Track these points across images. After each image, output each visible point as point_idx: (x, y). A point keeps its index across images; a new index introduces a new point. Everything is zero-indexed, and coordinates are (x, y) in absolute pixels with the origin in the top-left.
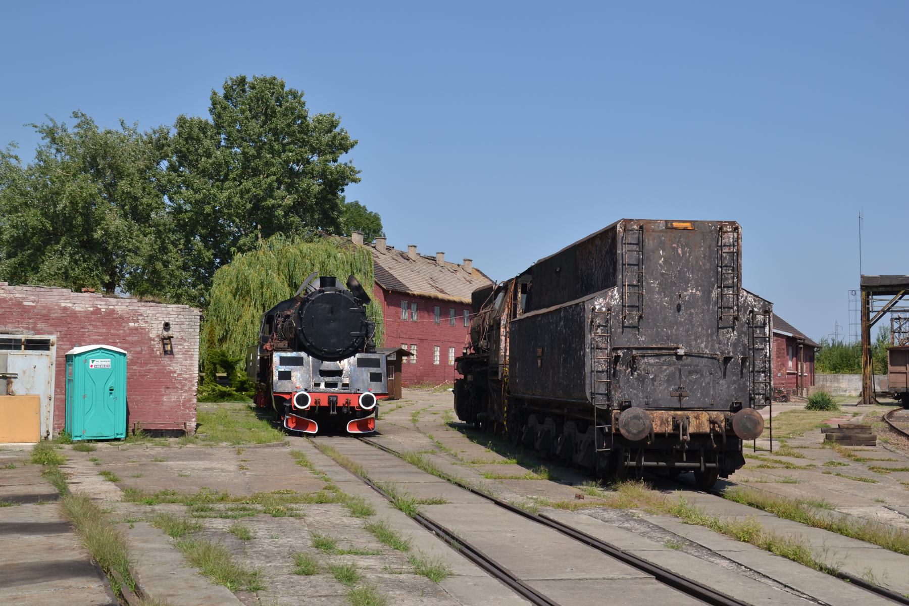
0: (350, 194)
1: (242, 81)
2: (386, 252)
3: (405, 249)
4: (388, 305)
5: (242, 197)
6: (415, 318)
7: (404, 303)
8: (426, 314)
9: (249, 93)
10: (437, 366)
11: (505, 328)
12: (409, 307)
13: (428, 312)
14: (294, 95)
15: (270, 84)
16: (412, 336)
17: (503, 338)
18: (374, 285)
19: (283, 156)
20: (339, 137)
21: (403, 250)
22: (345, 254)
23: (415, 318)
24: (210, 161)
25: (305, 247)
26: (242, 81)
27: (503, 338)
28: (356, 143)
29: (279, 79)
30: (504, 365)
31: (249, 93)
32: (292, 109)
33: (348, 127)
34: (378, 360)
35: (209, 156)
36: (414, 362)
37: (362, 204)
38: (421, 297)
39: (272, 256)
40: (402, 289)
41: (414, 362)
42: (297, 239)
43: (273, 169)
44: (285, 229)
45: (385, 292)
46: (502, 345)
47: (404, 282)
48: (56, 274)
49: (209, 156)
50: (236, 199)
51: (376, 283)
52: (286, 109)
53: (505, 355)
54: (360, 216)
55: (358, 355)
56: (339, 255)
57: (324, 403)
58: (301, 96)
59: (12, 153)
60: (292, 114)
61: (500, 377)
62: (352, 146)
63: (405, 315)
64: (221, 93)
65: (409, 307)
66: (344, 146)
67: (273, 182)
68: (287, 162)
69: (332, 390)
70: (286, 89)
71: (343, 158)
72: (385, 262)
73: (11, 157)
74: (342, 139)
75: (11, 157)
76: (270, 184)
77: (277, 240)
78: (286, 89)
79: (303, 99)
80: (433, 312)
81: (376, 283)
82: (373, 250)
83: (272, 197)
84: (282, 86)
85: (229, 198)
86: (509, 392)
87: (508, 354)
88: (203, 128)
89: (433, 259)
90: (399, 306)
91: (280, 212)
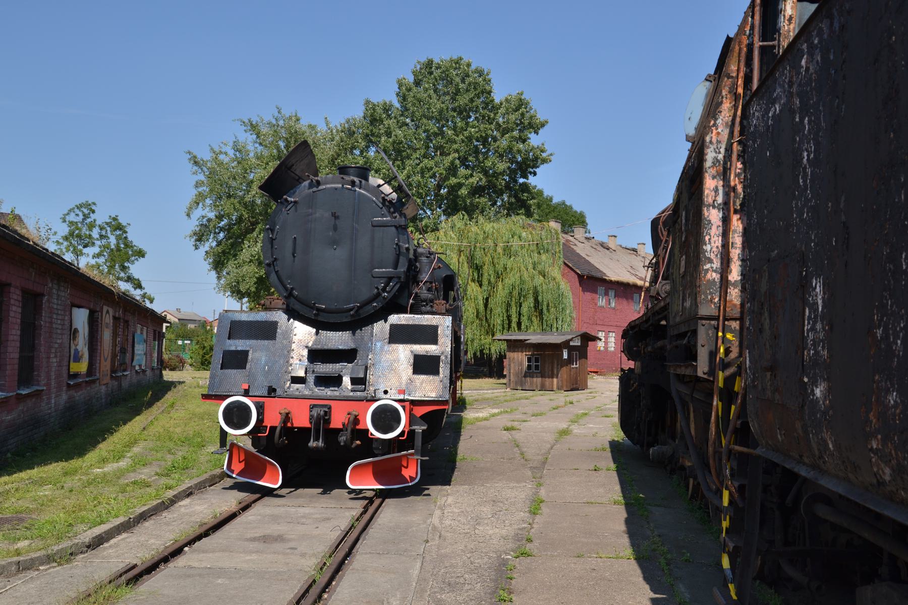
0: (541, 180)
1: (430, 63)
2: (585, 241)
3: (605, 239)
4: (584, 291)
5: (423, 177)
6: (613, 305)
7: (601, 289)
8: (625, 302)
9: (436, 73)
10: (613, 352)
11: (724, 174)
12: (606, 294)
13: (627, 299)
14: (480, 73)
15: (456, 63)
16: (610, 323)
17: (714, 216)
18: (562, 266)
19: (466, 133)
20: (528, 115)
21: (604, 241)
22: (531, 233)
23: (613, 305)
24: (391, 140)
25: (488, 227)
26: (430, 63)
27: (714, 216)
28: (547, 122)
29: (466, 60)
30: (720, 320)
31: (436, 73)
32: (476, 85)
33: (540, 109)
34: (435, 328)
35: (388, 134)
36: (613, 349)
37: (568, 203)
38: (619, 284)
39: (453, 236)
40: (599, 275)
41: (613, 349)
42: (481, 219)
43: (455, 146)
44: (471, 210)
45: (580, 277)
46: (712, 243)
47: (601, 269)
48: (251, 261)
49: (388, 134)
50: (418, 178)
51: (565, 264)
52: (470, 84)
53: (724, 282)
54: (567, 214)
55: (394, 319)
56: (524, 234)
57: (301, 420)
58: (488, 74)
59: (223, 150)
60: (475, 88)
61: (702, 367)
62: (543, 125)
63: (602, 302)
64: (411, 79)
65: (606, 294)
66: (536, 127)
67: (455, 159)
68: (470, 138)
69: (329, 392)
70: (473, 67)
71: (534, 140)
72: (582, 250)
73: (221, 153)
74: (531, 117)
75: (221, 153)
76: (452, 163)
77: (458, 220)
78: (473, 67)
79: (490, 77)
80: (632, 299)
81: (565, 264)
82: (571, 238)
83: (455, 175)
84: (469, 65)
85: (409, 177)
86: (743, 434)
87: (735, 275)
88: (387, 108)
89: (635, 250)
90: (595, 292)
91: (464, 191)
